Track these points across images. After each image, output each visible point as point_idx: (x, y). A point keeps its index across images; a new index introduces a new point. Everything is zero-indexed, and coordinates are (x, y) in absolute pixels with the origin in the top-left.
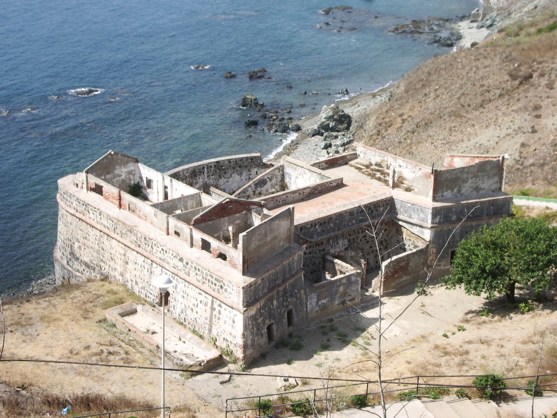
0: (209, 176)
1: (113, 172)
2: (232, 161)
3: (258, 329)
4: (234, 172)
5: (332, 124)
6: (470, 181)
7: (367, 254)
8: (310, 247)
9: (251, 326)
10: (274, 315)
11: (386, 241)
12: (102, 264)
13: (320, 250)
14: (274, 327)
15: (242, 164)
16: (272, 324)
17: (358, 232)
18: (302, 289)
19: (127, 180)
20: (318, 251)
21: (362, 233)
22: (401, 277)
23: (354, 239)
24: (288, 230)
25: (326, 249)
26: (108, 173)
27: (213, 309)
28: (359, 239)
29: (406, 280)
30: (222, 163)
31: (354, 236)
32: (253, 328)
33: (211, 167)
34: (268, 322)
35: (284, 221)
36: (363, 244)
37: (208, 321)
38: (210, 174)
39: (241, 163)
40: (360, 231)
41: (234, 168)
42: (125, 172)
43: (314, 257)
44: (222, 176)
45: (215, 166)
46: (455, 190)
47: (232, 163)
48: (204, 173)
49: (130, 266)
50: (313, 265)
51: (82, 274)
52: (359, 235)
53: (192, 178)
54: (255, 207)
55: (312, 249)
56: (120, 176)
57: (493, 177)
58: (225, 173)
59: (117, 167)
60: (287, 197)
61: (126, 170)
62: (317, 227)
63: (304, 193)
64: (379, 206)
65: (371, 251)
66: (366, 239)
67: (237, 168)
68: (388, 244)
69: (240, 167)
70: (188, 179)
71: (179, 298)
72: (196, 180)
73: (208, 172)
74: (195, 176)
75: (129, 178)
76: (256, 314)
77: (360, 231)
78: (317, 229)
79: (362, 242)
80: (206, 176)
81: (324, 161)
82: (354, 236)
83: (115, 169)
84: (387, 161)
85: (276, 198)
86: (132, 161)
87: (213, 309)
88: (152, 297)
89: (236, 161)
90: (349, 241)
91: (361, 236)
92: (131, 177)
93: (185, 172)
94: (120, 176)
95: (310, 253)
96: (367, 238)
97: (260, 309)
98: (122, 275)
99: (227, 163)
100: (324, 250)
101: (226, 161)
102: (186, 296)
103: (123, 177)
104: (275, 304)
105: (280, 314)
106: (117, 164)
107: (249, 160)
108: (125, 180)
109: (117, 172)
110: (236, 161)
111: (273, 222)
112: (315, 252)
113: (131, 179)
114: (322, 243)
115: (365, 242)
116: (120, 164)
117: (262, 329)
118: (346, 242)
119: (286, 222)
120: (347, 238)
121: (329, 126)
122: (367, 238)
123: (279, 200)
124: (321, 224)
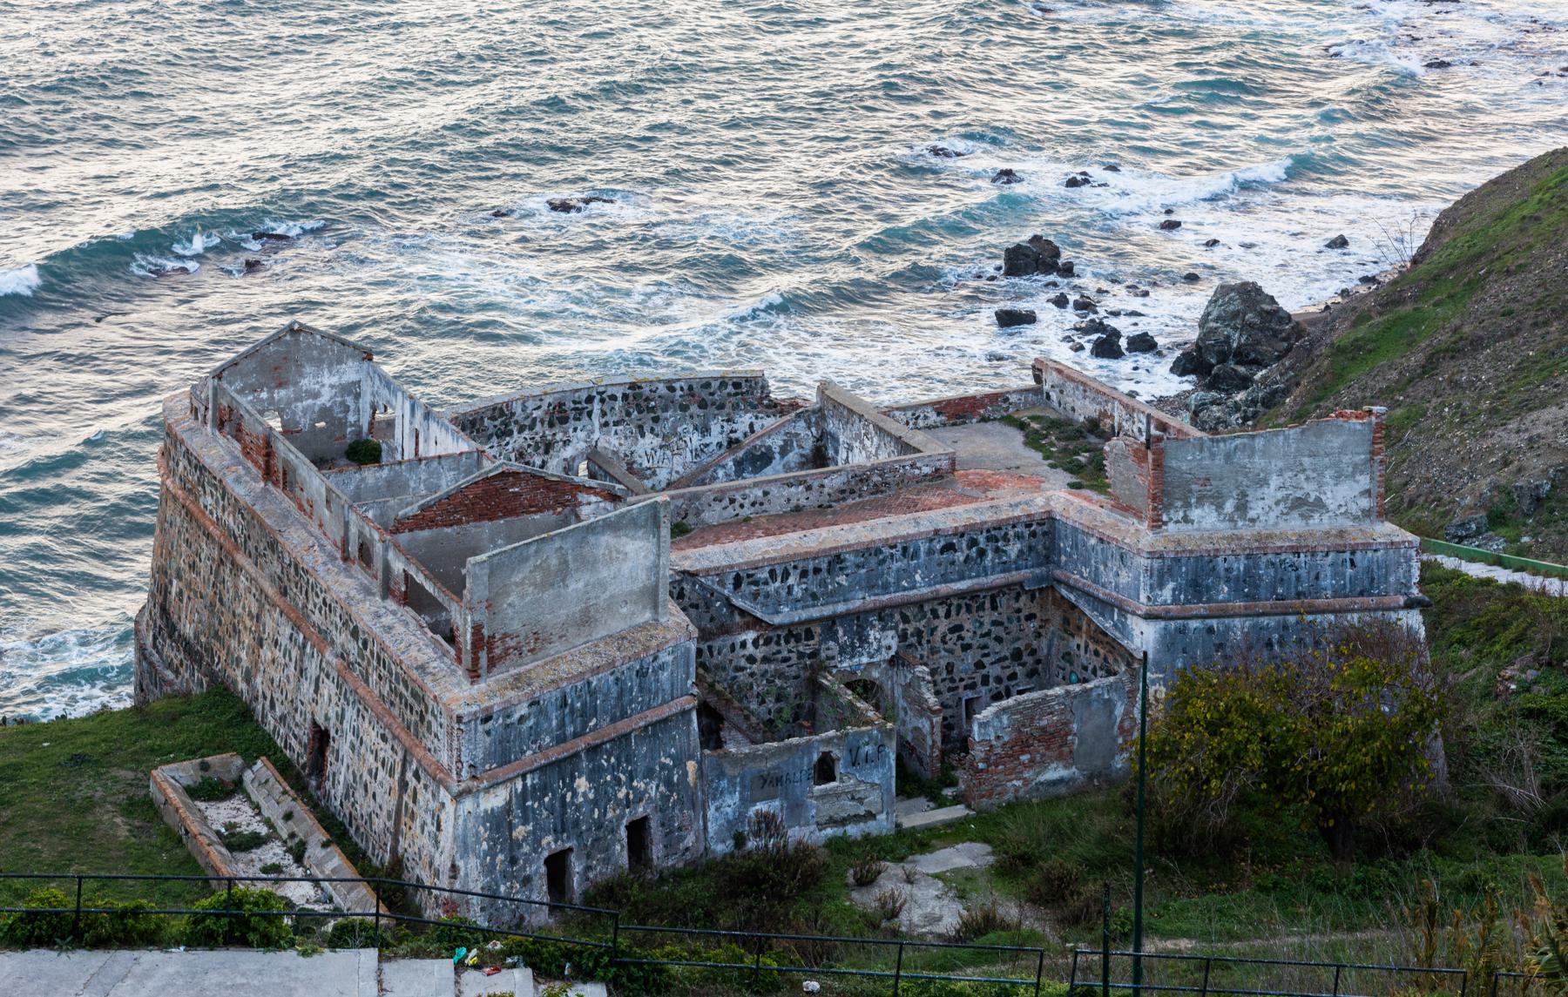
0: (606, 424)
1: (296, 384)
2: (677, 385)
3: (513, 861)
4: (682, 420)
5: (1237, 339)
6: (1275, 481)
7: (966, 688)
8: (768, 642)
9: (485, 846)
10: (576, 823)
11: (1033, 652)
12: (216, 645)
13: (801, 655)
14: (576, 866)
15: (709, 398)
16: (570, 850)
17: (935, 613)
18: (691, 757)
19: (337, 410)
20: (794, 656)
21: (948, 615)
22: (1044, 765)
23: (919, 633)
24: (649, 569)
25: (823, 655)
26: (280, 385)
27: (404, 785)
28: (938, 634)
29: (1061, 781)
30: (646, 390)
31: (921, 625)
32: (491, 852)
33: (613, 398)
34: (550, 844)
35: (634, 538)
36: (951, 651)
37: (390, 824)
38: (611, 419)
39: (704, 394)
40: (942, 611)
41: (684, 408)
42: (332, 386)
43: (781, 675)
44: (647, 429)
45: (625, 397)
47: (679, 393)
48: (590, 414)
49: (266, 653)
50: (778, 700)
51: (177, 673)
52: (936, 622)
53: (551, 425)
54: (593, 499)
55: (774, 648)
56: (316, 395)
57: (1353, 475)
58: (656, 420)
59: (308, 369)
60: (766, 493)
61: (334, 380)
62: (791, 581)
63: (822, 486)
64: (1006, 538)
65: (978, 680)
66: (960, 638)
67: (694, 409)
68: (1038, 662)
69: (703, 405)
70: (538, 427)
71: (345, 749)
72: (565, 433)
73: (604, 414)
75: (343, 403)
76: (507, 809)
77: (942, 611)
78: (790, 588)
79: (950, 645)
80: (597, 425)
81: (932, 404)
82: (921, 625)
83: (302, 376)
84: (1112, 417)
85: (730, 494)
86: (354, 357)
87: (404, 785)
88: (297, 748)
89: (691, 388)
90: (903, 637)
91: (943, 625)
92: (350, 401)
93: (531, 405)
94: (316, 395)
95: (765, 660)
96: (963, 633)
97: (524, 796)
98: (248, 678)
100: (814, 655)
101: (661, 386)
102: (357, 744)
103: (325, 399)
104: (581, 790)
105: (600, 826)
107: (730, 389)
108: (330, 409)
109: (306, 383)
110: (691, 388)
111: (592, 539)
112: (786, 660)
113: (347, 409)
114: (809, 635)
115: (958, 648)
116: (319, 363)
118: (891, 640)
119: (639, 543)
120: (895, 628)
121: (1229, 345)
122: (963, 633)
123: (738, 497)
124: (804, 574)
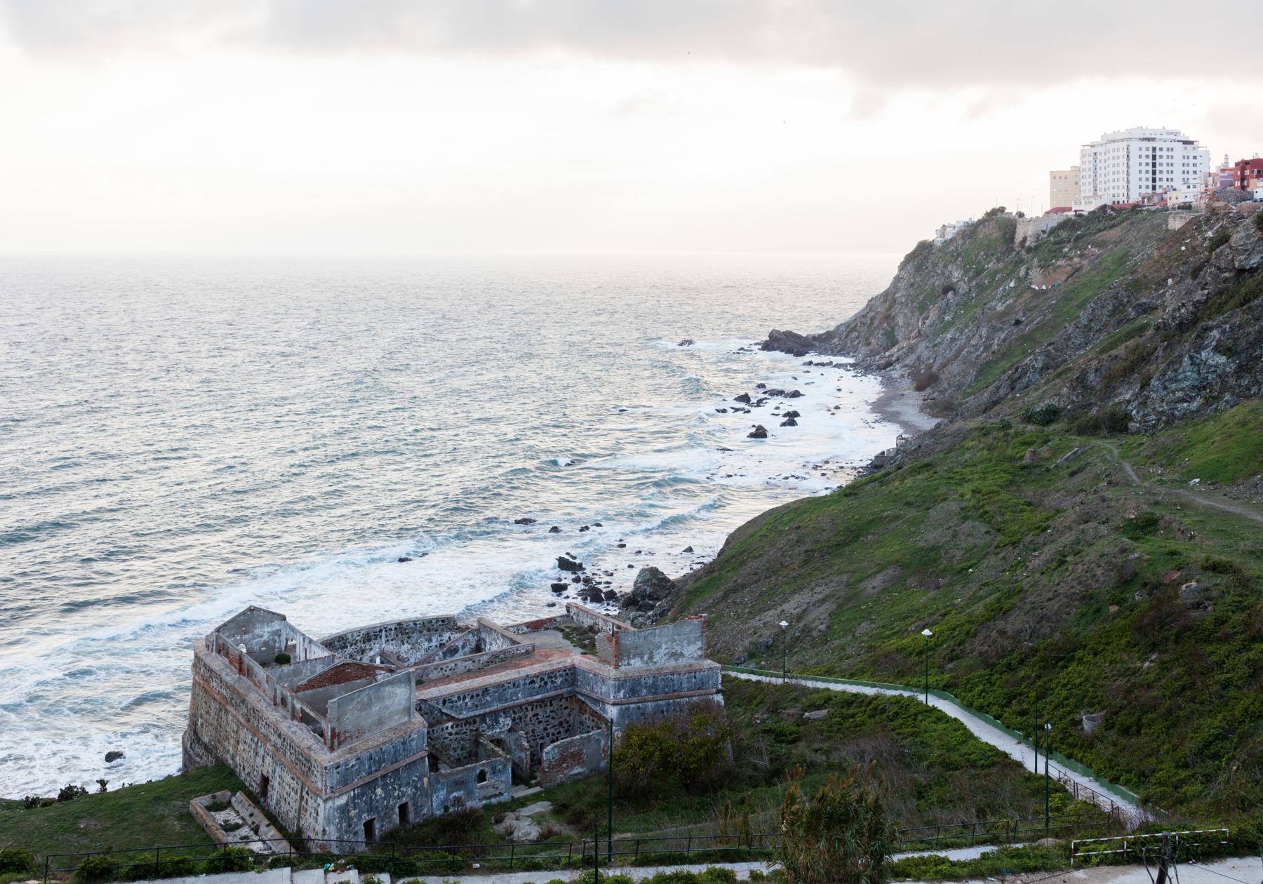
3: (350, 825)
6: (664, 646)
14: (377, 825)
22: (572, 767)
23: (520, 718)
27: (302, 798)
32: (341, 823)
34: (365, 817)
43: (463, 739)
46: (646, 657)
69: (429, 630)
71: (276, 785)
74: (369, 640)
76: (347, 804)
87: (302, 798)
90: (514, 720)
91: (530, 714)
97: (354, 798)
98: (233, 759)
99: (411, 625)
103: (265, 638)
106: (259, 622)
114: (475, 722)
116: (262, 622)
117: (356, 825)
118: (509, 722)
